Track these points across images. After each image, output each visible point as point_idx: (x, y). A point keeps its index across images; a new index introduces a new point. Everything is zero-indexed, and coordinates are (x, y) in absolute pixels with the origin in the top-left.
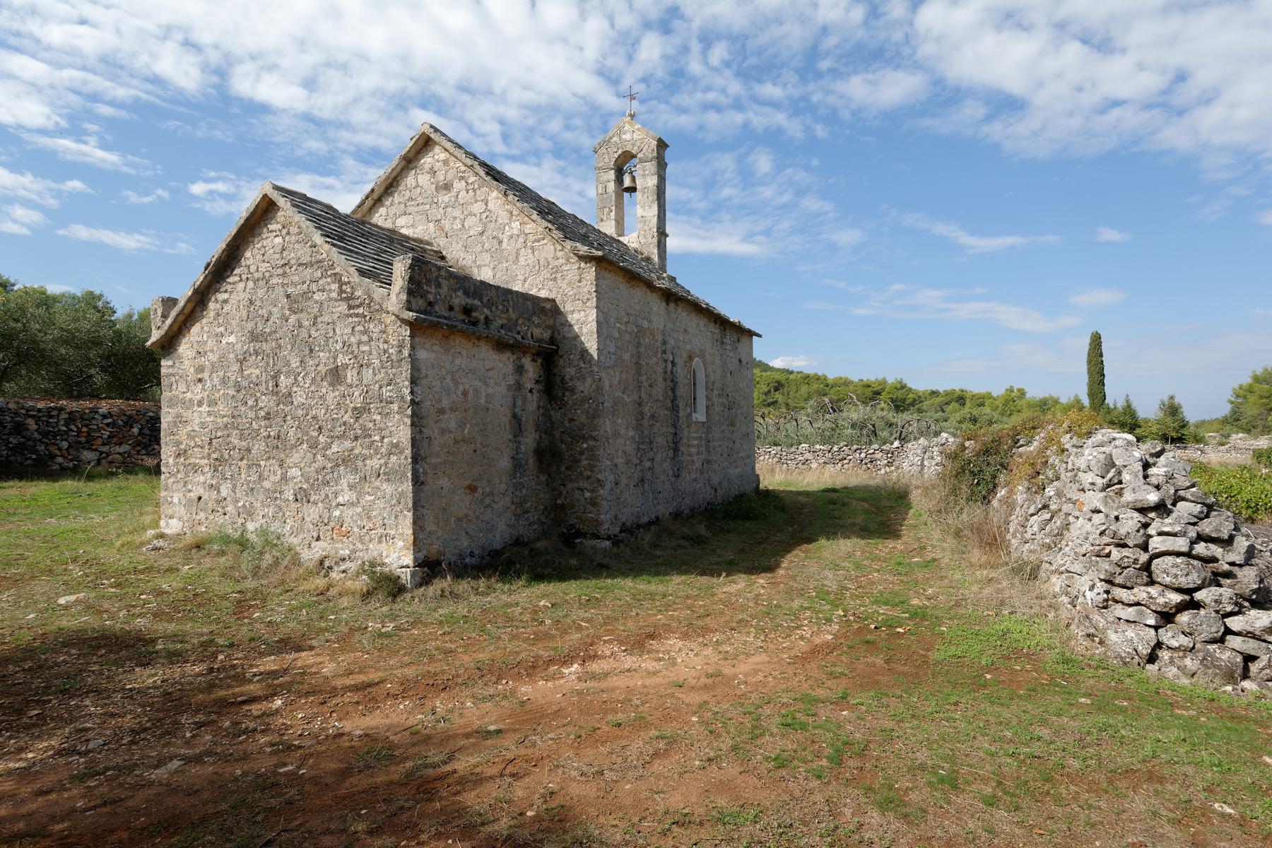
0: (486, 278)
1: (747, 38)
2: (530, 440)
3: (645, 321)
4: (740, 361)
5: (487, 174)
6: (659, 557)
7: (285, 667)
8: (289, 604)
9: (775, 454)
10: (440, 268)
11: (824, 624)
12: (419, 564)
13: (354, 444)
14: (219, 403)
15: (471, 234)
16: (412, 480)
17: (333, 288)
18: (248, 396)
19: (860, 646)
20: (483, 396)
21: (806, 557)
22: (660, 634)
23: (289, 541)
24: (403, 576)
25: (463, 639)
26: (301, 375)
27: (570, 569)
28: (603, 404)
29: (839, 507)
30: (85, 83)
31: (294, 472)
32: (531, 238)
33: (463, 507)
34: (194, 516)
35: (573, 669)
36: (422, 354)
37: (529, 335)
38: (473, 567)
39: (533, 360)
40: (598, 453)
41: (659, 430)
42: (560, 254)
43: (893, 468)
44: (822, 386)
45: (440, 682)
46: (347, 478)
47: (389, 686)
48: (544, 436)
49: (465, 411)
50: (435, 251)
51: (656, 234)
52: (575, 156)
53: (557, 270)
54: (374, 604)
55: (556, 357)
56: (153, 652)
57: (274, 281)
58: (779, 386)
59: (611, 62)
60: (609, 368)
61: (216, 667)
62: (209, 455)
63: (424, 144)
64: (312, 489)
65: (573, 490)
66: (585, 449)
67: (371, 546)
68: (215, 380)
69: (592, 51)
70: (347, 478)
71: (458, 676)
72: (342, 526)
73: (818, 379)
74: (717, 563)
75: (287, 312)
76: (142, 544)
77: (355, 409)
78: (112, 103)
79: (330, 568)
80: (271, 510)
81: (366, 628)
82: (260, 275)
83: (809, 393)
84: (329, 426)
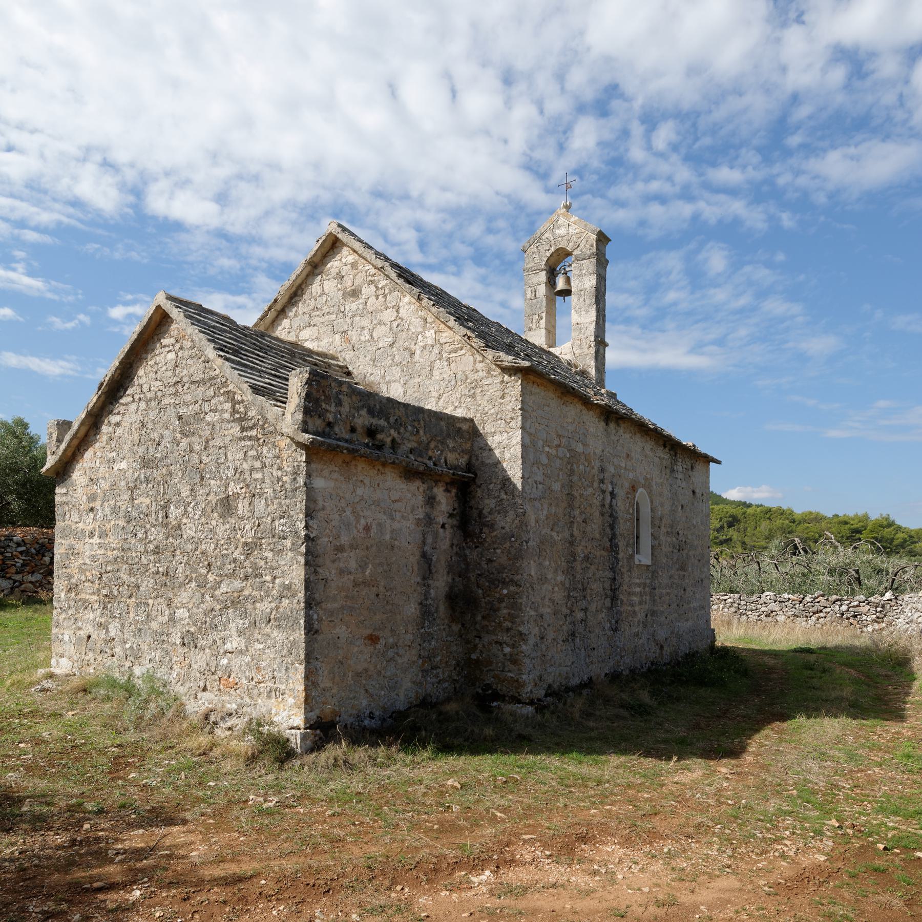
0: (396, 395)
1: (698, 114)
2: (441, 583)
3: (580, 445)
4: (694, 492)
5: (399, 276)
6: (592, 729)
7: (152, 844)
8: (168, 765)
9: (732, 603)
10: (341, 384)
11: (813, 838)
12: (313, 725)
13: (244, 584)
14: (110, 534)
15: (380, 346)
16: (305, 628)
17: (226, 408)
18: (138, 527)
19: (866, 875)
20: (388, 532)
21: (781, 740)
22: (594, 836)
23: (175, 690)
24: (292, 739)
25: (354, 824)
26: (191, 505)
27: (485, 739)
28: (527, 542)
29: (819, 674)
30: (12, 209)
31: (181, 613)
32: (447, 348)
33: (362, 660)
34: (83, 656)
35: (484, 877)
36: (319, 483)
37: (443, 461)
38: (373, 731)
39: (447, 490)
40: (520, 601)
41: (594, 574)
42: (480, 366)
43: (884, 625)
44: (787, 522)
45: (322, 882)
46: (236, 623)
47: (263, 882)
48: (457, 579)
49: (367, 548)
50: (340, 367)
51: (593, 344)
52: (497, 262)
53: (476, 384)
54: (259, 769)
55: (473, 487)
56: (18, 815)
57: (166, 401)
58: (733, 522)
59: (538, 154)
60: (535, 499)
61: (79, 839)
62: (99, 590)
63: (332, 246)
64: (200, 633)
65: (490, 643)
66: (506, 595)
67: (260, 701)
68: (106, 509)
69: (518, 141)
70: (236, 623)
71: (344, 875)
72: (229, 676)
73: (782, 514)
74: (665, 741)
75: (179, 436)
76: (32, 684)
77: (246, 544)
78: (37, 229)
79: (216, 723)
80: (158, 654)
81: (247, 801)
82: (152, 395)
83: (770, 530)
84: (219, 563)
